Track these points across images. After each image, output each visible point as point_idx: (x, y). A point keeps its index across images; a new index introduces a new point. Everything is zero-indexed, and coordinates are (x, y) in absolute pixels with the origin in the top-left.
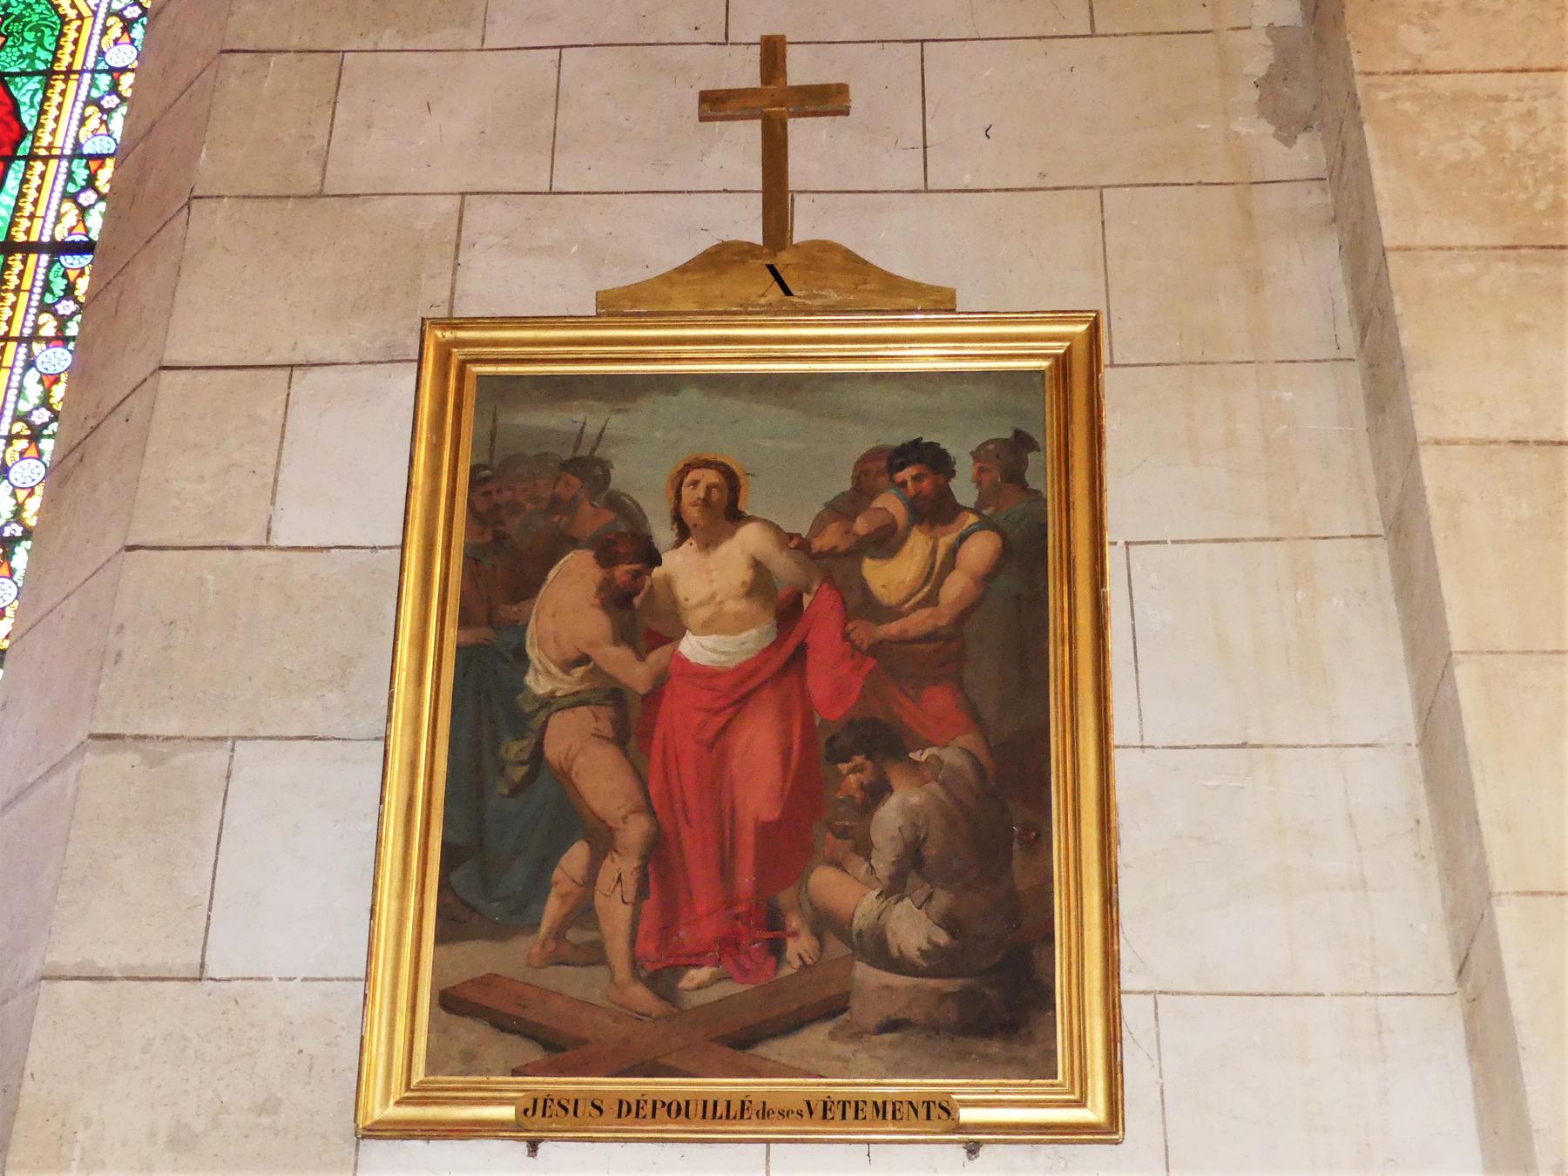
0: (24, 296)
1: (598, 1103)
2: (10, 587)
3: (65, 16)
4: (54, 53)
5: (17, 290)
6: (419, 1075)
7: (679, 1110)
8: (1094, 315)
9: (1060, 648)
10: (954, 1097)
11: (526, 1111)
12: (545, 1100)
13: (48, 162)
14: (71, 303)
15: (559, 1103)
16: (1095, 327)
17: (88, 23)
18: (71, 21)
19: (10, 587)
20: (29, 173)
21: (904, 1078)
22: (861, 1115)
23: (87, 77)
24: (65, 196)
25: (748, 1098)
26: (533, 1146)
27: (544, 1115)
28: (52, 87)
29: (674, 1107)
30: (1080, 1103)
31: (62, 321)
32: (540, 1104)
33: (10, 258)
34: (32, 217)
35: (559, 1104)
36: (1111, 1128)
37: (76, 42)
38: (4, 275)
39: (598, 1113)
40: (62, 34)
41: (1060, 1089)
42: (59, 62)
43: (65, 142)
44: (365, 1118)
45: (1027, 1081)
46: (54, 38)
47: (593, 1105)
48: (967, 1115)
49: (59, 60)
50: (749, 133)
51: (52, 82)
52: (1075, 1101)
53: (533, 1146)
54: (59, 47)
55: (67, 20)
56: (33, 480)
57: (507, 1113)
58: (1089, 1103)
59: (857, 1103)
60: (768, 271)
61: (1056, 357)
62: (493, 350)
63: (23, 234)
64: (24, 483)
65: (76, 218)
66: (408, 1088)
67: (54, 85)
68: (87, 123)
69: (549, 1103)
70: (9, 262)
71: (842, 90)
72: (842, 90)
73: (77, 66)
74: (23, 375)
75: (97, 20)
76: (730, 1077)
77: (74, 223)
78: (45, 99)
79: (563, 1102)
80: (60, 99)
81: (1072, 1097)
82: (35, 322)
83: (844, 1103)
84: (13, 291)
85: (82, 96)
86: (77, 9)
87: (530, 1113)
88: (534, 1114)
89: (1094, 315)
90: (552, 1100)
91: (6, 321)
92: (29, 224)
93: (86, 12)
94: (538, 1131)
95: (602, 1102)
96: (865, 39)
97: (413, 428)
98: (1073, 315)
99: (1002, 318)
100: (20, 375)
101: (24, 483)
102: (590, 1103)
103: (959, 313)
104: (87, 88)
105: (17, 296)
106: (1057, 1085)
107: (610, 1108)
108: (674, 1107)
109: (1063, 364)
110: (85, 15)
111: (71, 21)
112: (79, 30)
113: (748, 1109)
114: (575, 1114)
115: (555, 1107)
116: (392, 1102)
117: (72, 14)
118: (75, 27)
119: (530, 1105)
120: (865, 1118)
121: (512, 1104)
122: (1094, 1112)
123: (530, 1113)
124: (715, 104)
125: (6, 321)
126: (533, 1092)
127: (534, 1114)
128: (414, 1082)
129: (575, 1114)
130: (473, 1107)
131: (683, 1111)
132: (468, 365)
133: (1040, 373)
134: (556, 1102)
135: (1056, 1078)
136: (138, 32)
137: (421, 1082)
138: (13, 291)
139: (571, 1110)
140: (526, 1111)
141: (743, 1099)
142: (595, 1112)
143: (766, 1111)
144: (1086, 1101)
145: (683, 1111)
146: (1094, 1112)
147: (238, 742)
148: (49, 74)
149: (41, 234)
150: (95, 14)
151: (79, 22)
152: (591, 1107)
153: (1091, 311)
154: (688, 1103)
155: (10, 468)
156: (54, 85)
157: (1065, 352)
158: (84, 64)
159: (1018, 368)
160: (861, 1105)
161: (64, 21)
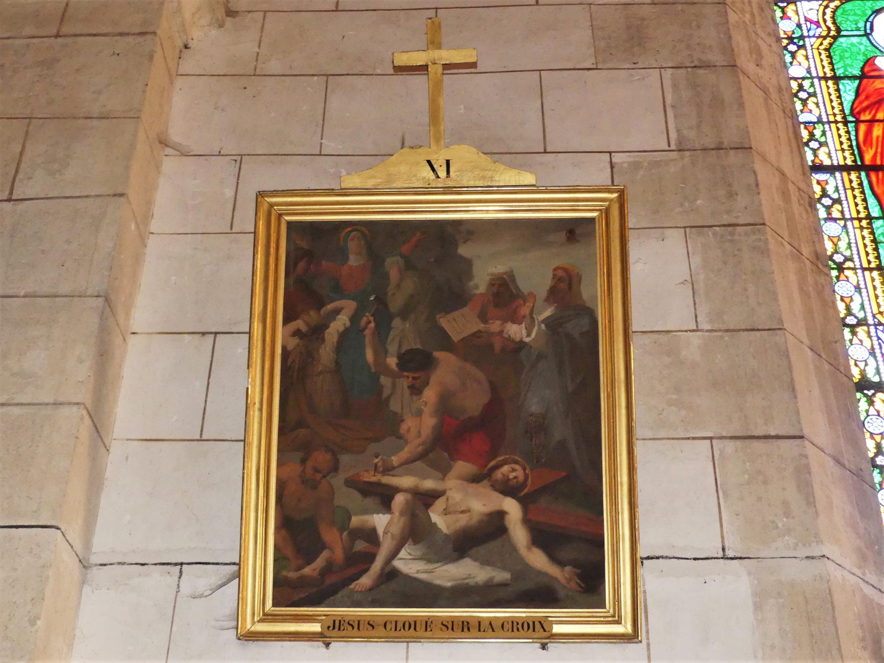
2: (827, 230)
7: (427, 624)
11: (329, 627)
14: (837, 261)
15: (348, 623)
19: (827, 230)
22: (342, 628)
24: (814, 95)
25: (343, 619)
27: (339, 630)
30: (619, 622)
31: (801, 88)
36: (632, 638)
37: (831, 101)
39: (351, 628)
47: (442, 624)
48: (557, 629)
52: (614, 621)
56: (871, 419)
57: (316, 627)
63: (830, 6)
64: (877, 419)
65: (867, 372)
68: (810, 84)
74: (858, 281)
77: (839, 243)
82: (851, 251)
85: (819, 96)
88: (334, 628)
91: (860, 212)
96: (306, 13)
101: (877, 419)
102: (367, 624)
104: (808, 54)
107: (508, 626)
109: (607, 211)
113: (343, 625)
115: (346, 625)
120: (344, 630)
121: (319, 623)
122: (626, 628)
127: (334, 628)
129: (359, 629)
130: (284, 624)
131: (413, 627)
133: (592, 220)
135: (605, 608)
136: (794, 85)
139: (450, 627)
140: (329, 627)
141: (427, 620)
142: (370, 628)
145: (413, 627)
147: (268, 14)
151: (820, 47)
154: (415, 622)
155: (870, 354)
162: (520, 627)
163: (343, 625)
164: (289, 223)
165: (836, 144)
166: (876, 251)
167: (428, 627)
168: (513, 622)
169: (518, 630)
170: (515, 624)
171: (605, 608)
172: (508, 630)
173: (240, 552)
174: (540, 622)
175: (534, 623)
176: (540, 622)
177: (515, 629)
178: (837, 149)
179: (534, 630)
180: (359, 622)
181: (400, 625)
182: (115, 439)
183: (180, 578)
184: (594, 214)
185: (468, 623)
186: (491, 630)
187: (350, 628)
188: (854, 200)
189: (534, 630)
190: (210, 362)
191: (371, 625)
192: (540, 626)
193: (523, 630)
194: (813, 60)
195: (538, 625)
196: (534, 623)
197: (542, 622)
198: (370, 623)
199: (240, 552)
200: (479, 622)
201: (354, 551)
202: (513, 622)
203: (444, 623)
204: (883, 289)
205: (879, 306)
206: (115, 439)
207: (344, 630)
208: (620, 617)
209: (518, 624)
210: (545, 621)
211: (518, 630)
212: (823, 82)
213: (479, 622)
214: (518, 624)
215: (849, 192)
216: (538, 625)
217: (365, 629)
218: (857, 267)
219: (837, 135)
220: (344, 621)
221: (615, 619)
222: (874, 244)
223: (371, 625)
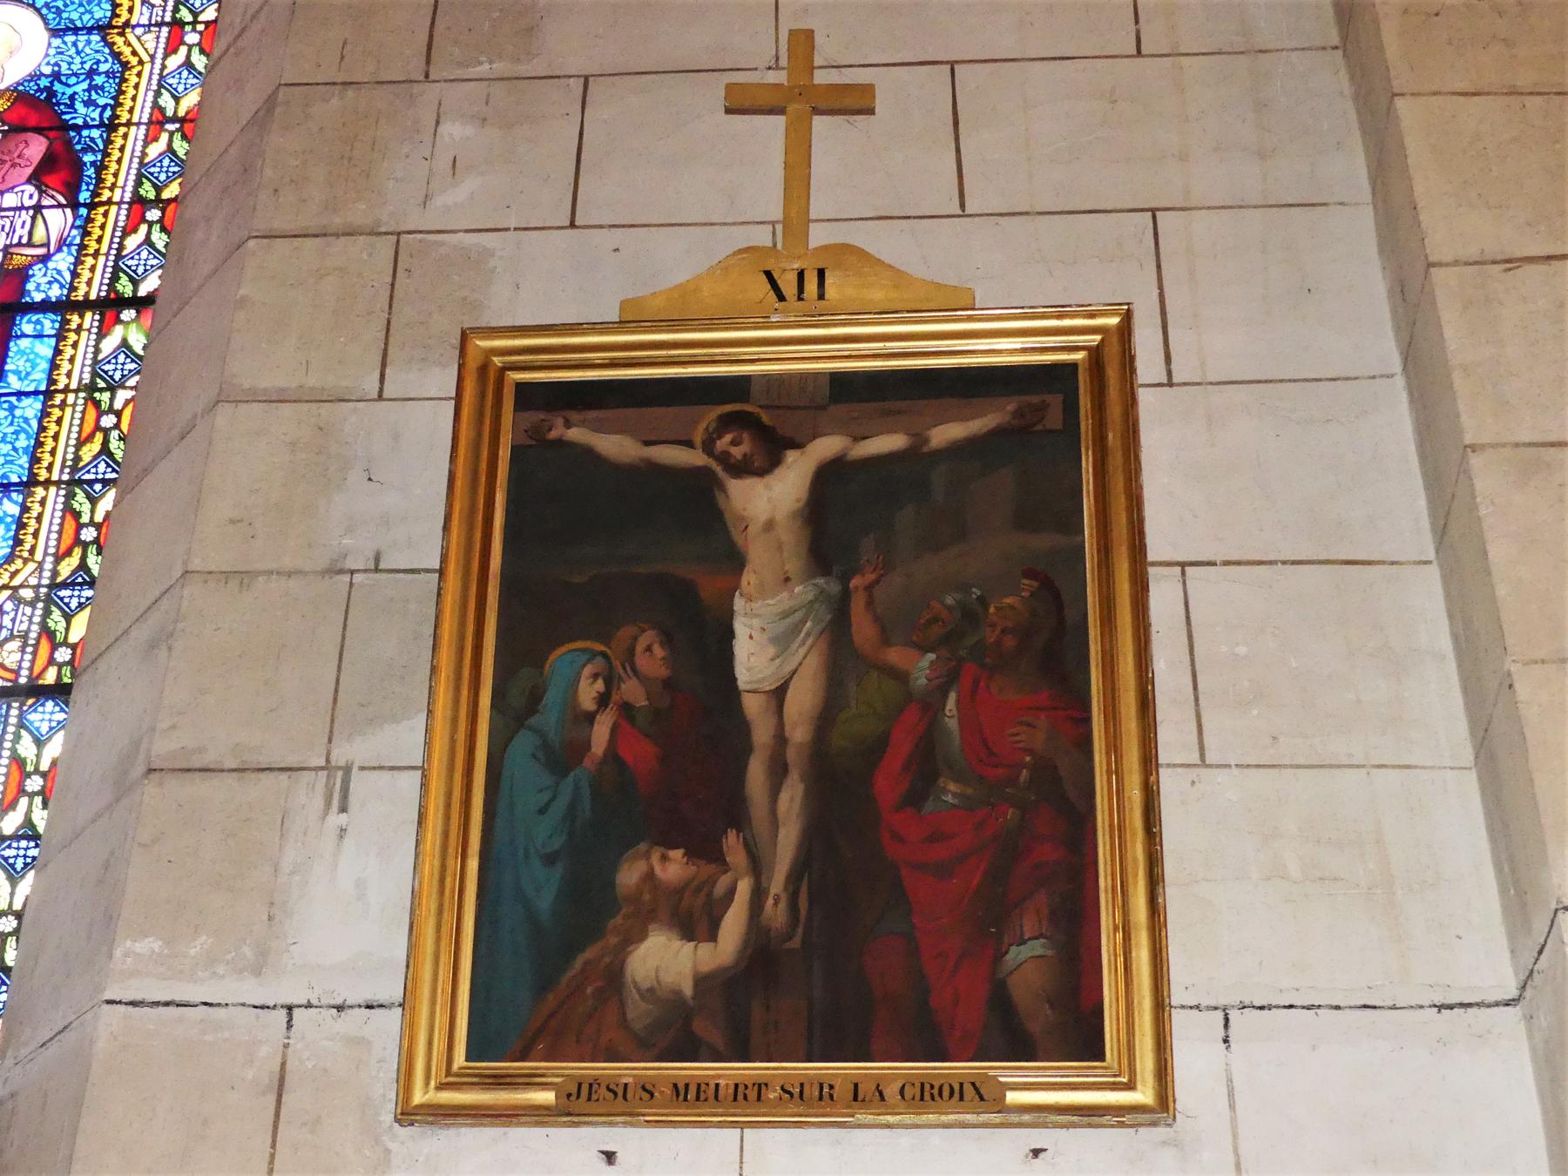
0: (102, 259)
1: (649, 1087)
3: (128, 62)
4: (115, 98)
6: (460, 1059)
8: (1126, 307)
9: (454, 864)
10: (1001, 1079)
11: (569, 1095)
12: (591, 1085)
13: (84, 315)
17: (147, 67)
18: (133, 67)
20: (77, 280)
22: (594, 1097)
23: (74, 386)
27: (589, 1099)
28: (82, 263)
29: (946, 1093)
30: (1130, 1086)
33: (93, 212)
34: (96, 254)
38: (101, 174)
40: (124, 80)
41: (1109, 1072)
42: (79, 277)
46: (90, 193)
48: (1013, 1097)
49: (75, 289)
51: (83, 259)
52: (1125, 1084)
54: (120, 92)
55: (129, 66)
57: (547, 1097)
58: (1139, 1086)
59: (699, 1085)
62: (536, 357)
66: (448, 1073)
67: (84, 261)
69: (595, 1087)
70: (54, 377)
71: (868, 90)
72: (868, 90)
73: (135, 119)
75: (155, 66)
76: (673, 1061)
80: (123, 142)
83: (760, 1085)
84: (74, 331)
86: (139, 56)
88: (578, 1097)
89: (1126, 307)
90: (599, 1084)
91: (113, 174)
92: (93, 262)
93: (146, 58)
95: (654, 1086)
97: (453, 439)
100: (78, 425)
105: (62, 410)
106: (1105, 1068)
108: (946, 1093)
109: (1095, 353)
110: (145, 61)
111: (133, 67)
112: (139, 75)
114: (625, 1098)
115: (603, 1091)
116: (433, 1083)
117: (134, 61)
118: (136, 72)
122: (1143, 1095)
123: (573, 1098)
125: (113, 174)
127: (578, 1097)
128: (455, 1067)
129: (625, 1098)
133: (1073, 366)
134: (603, 1087)
135: (1103, 1059)
137: (460, 1068)
138: (74, 331)
139: (620, 1094)
140: (569, 1095)
142: (646, 1096)
145: (957, 1095)
146: (1143, 1095)
148: (48, 394)
149: (140, 118)
150: (152, 57)
151: (139, 68)
152: (641, 1090)
156: (84, 261)
157: (1098, 345)
158: (140, 118)
160: (703, 1087)
161: (126, 66)
162: (936, 1092)
163: (596, 1092)
164: (521, 387)
167: (702, 1094)
168: (922, 1084)
169: (933, 1098)
170: (927, 1087)
171: (1103, 1059)
172: (913, 1099)
173: (633, 322)
174: (973, 1084)
175: (961, 1085)
176: (973, 1084)
179: (961, 1099)
181: (752, 1094)
184: (1079, 356)
185: (831, 1087)
186: (878, 1098)
187: (610, 1095)
189: (961, 1099)
190: (381, 352)
195: (968, 1089)
196: (961, 1085)
197: (978, 1085)
198: (611, 1087)
199: (633, 322)
200: (856, 1085)
202: (922, 1084)
203: (786, 1087)
207: (706, 1100)
209: (932, 1087)
210: (982, 1083)
211: (933, 1098)
213: (856, 1085)
214: (932, 1087)
216: (968, 1089)
217: (637, 1097)
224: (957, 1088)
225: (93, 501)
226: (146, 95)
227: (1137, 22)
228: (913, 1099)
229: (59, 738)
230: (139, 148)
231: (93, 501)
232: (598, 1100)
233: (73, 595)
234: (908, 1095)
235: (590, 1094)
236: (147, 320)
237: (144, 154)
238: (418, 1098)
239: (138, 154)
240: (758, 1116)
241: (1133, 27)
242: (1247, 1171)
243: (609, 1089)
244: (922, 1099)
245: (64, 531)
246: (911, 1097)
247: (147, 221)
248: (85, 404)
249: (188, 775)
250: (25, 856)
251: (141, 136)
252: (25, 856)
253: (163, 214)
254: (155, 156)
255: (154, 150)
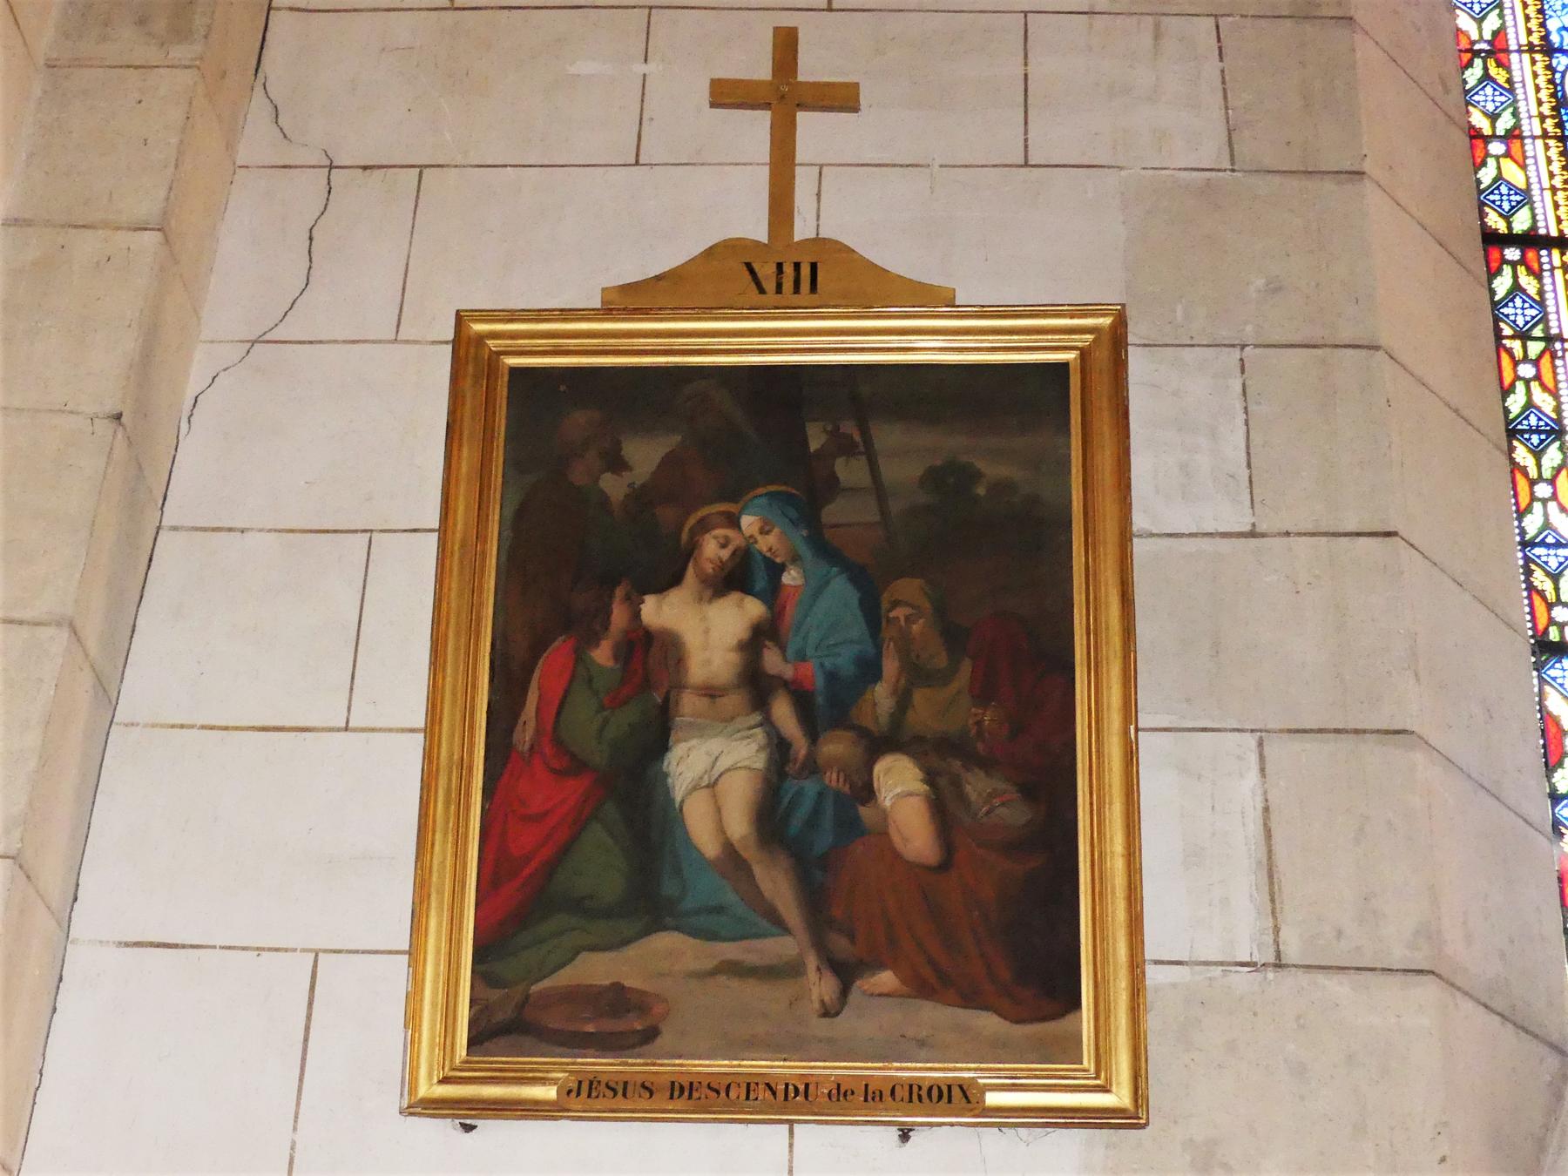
5: (1553, 269)
11: (569, 1092)
16: (1121, 321)
21: (605, 1058)
22: (752, 1096)
26: (905, 1136)
27: (589, 1096)
29: (935, 1093)
30: (1105, 1089)
32: (585, 1087)
35: (608, 1086)
36: (1129, 1119)
42: (1563, 166)
43: (1530, 124)
44: (415, 1098)
45: (881, 1065)
48: (993, 1099)
50: (755, 127)
52: (1098, 1086)
53: (905, 1136)
57: (549, 1093)
58: (1114, 1088)
60: (745, 268)
61: (1081, 349)
71: (854, 88)
78: (1551, 81)
79: (611, 1084)
81: (1098, 1082)
87: (574, 1094)
88: (578, 1094)
89: (1119, 307)
90: (599, 1082)
94: (598, 1112)
98: (1013, 309)
99: (1101, 310)
103: (958, 306)
108: (935, 1093)
113: (596, 1088)
115: (603, 1088)
119: (575, 1086)
120: (597, 1097)
122: (1119, 1097)
123: (574, 1094)
124: (727, 95)
126: (622, 1075)
127: (578, 1094)
129: (624, 1095)
132: (502, 357)
134: (603, 1085)
140: (569, 1092)
143: (842, 1091)
144: (1111, 1085)
152: (707, 1090)
153: (1117, 305)
159: (978, 361)
162: (924, 1093)
163: (596, 1088)
164: (515, 372)
165: (1519, 28)
166: (1559, 128)
170: (915, 1089)
172: (902, 1100)
174: (961, 1087)
175: (949, 1087)
177: (915, 1097)
178: (1544, 187)
179: (950, 1101)
180: (626, 1083)
182: (175, 529)
183: (19, 28)
184: (1070, 356)
187: (610, 1093)
188: (1526, 23)
189: (950, 1101)
191: (647, 1088)
192: (961, 1094)
193: (931, 1100)
194: (1514, 29)
195: (956, 1092)
196: (949, 1087)
201: (471, 325)
202: (911, 1086)
204: (1565, 177)
205: (1559, 220)
206: (175, 529)
207: (597, 1097)
208: (1109, 1080)
209: (920, 1088)
211: (920, 1097)
212: (1526, 57)
214: (920, 1088)
215: (1548, 194)
216: (956, 1092)
218: (1524, 134)
219: (1535, 100)
220: (599, 1082)
221: (1098, 1082)
222: (1550, 73)
223: (647, 1088)
224: (801, 1088)
225: (1538, 454)
226: (1523, 76)
227: (818, 219)
228: (902, 1100)
229: (1471, 82)
230: (1509, 18)
231: (1538, 454)
232: (699, 1098)
233: (1523, 314)
234: (898, 1097)
235: (590, 1088)
236: (1464, 44)
237: (1501, 16)
238: (424, 1091)
239: (1507, 12)
240: (823, 1115)
241: (820, 223)
242: (1153, 1124)
243: (608, 1086)
244: (911, 1101)
245: (1551, 370)
246: (900, 1099)
247: (1539, 500)
248: (1541, 264)
249: (1450, 756)
250: (1523, 309)
251: (1511, 32)
252: (1509, 195)
253: (1532, 493)
254: (1490, 15)
255: (1492, 22)
